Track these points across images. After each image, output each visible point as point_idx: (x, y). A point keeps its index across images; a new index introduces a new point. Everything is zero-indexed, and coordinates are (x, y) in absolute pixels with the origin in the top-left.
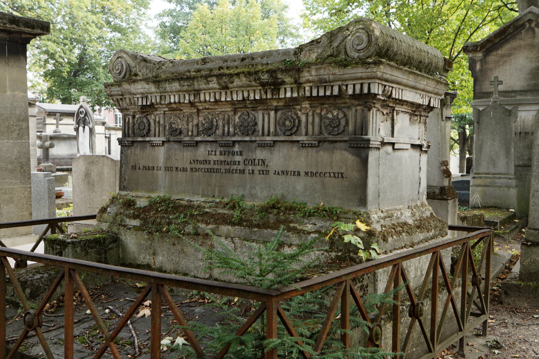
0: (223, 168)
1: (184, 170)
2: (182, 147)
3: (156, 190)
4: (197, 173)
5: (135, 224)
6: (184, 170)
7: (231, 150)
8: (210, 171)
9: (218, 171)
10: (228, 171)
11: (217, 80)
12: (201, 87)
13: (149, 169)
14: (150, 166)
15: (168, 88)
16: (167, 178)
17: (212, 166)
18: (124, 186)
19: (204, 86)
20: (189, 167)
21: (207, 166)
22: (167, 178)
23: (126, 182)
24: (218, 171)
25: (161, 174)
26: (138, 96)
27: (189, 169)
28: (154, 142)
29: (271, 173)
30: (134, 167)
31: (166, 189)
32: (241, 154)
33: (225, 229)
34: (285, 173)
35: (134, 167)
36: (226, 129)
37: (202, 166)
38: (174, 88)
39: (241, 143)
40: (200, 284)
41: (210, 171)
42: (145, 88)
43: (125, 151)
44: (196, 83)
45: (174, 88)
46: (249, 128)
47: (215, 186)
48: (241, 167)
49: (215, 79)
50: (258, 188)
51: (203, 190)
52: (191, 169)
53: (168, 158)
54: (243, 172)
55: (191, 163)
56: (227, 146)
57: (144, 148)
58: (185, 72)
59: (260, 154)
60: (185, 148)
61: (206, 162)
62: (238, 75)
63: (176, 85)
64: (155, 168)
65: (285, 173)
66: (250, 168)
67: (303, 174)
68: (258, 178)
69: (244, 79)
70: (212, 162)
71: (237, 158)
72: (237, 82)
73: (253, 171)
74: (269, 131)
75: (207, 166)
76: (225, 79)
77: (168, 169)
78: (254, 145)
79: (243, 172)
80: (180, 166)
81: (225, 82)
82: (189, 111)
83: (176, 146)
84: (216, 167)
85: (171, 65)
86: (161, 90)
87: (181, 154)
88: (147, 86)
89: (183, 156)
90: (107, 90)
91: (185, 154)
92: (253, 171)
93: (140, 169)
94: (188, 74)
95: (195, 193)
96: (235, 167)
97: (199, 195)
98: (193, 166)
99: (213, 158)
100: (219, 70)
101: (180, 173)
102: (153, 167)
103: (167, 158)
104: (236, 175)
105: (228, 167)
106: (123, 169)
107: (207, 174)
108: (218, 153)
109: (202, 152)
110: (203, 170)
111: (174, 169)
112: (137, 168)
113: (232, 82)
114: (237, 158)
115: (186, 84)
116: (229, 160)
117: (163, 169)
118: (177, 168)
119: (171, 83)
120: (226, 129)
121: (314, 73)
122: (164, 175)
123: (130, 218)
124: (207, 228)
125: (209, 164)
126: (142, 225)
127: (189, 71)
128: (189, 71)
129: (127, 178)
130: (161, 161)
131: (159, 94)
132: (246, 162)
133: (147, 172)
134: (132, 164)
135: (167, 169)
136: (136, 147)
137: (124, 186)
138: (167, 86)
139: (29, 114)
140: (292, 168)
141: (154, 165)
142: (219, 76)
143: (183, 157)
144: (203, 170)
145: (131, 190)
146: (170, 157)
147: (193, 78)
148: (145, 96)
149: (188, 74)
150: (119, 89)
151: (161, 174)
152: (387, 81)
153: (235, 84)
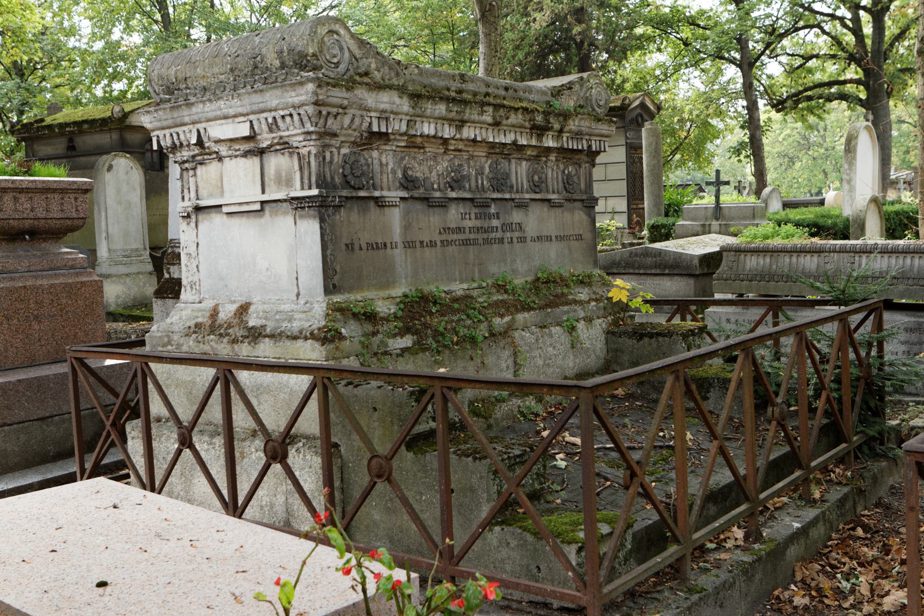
0: (481, 236)
1: (432, 244)
2: (426, 207)
3: (394, 282)
4: (450, 248)
5: (403, 345)
6: (432, 244)
7: (486, 210)
8: (466, 243)
9: (475, 242)
10: (487, 242)
11: (494, 112)
12: (472, 117)
13: (378, 248)
14: (379, 241)
15: (429, 111)
16: (409, 260)
17: (467, 236)
18: (334, 286)
19: (475, 117)
20: (438, 239)
21: (461, 237)
22: (409, 260)
23: (336, 278)
24: (475, 242)
25: (398, 254)
26: (373, 114)
27: (439, 243)
28: (387, 199)
29: (529, 239)
30: (350, 247)
31: (409, 279)
32: (498, 218)
33: (521, 317)
34: (539, 238)
35: (350, 247)
36: (480, 182)
37: (455, 237)
38: (437, 111)
39: (497, 202)
40: (602, 384)
41: (466, 243)
42: (394, 103)
43: (329, 216)
44: (468, 111)
45: (437, 111)
46: (500, 182)
47: (474, 265)
48: (499, 235)
49: (491, 109)
50: (518, 261)
51: (460, 272)
52: (442, 242)
53: (407, 227)
54: (501, 241)
55: (440, 233)
56: (480, 204)
57: (365, 211)
58: (443, 89)
59: (517, 216)
60: (431, 209)
61: (459, 230)
62: (517, 109)
63: (441, 109)
64: (389, 245)
65: (539, 238)
66: (508, 235)
67: (554, 238)
68: (517, 246)
69: (520, 116)
70: (467, 230)
71: (495, 223)
72: (514, 119)
73: (512, 238)
74: (522, 187)
75: (461, 237)
76: (502, 112)
77: (409, 245)
78: (511, 204)
79: (501, 241)
80: (426, 240)
81: (501, 116)
82: (434, 150)
83: (419, 206)
84: (472, 236)
85: (416, 71)
86: (418, 111)
87: (426, 219)
88: (397, 100)
89: (429, 221)
90: (319, 91)
91: (431, 219)
92: (512, 238)
93: (361, 249)
94: (447, 93)
95: (451, 279)
96: (493, 235)
97: (455, 281)
98: (444, 237)
99: (468, 224)
100: (485, 97)
101: (428, 252)
102: (385, 245)
103: (405, 226)
104: (495, 246)
105: (485, 236)
106: (329, 252)
107: (463, 248)
108: (473, 216)
109: (454, 214)
110: (457, 243)
111: (418, 244)
112: (356, 247)
113: (507, 118)
114: (495, 223)
115: (455, 109)
116: (486, 226)
117: (400, 245)
118: (422, 242)
119: (436, 104)
120: (480, 182)
121: (576, 123)
122: (403, 256)
123: (395, 336)
124: (499, 322)
125: (464, 232)
126: (418, 343)
127: (448, 89)
128: (448, 89)
129: (338, 269)
130: (397, 233)
131: (408, 118)
132: (504, 228)
133: (375, 253)
134: (345, 240)
135: (407, 244)
136: (351, 209)
137: (334, 286)
138: (430, 107)
139: (594, 179)
140: (545, 233)
141: (386, 240)
142: (497, 107)
143: (430, 223)
144: (457, 243)
145: (350, 290)
146: (410, 224)
147: (465, 102)
148: (384, 116)
149: (447, 93)
150: (345, 95)
151: (398, 254)
152: (602, 136)
153: (510, 121)
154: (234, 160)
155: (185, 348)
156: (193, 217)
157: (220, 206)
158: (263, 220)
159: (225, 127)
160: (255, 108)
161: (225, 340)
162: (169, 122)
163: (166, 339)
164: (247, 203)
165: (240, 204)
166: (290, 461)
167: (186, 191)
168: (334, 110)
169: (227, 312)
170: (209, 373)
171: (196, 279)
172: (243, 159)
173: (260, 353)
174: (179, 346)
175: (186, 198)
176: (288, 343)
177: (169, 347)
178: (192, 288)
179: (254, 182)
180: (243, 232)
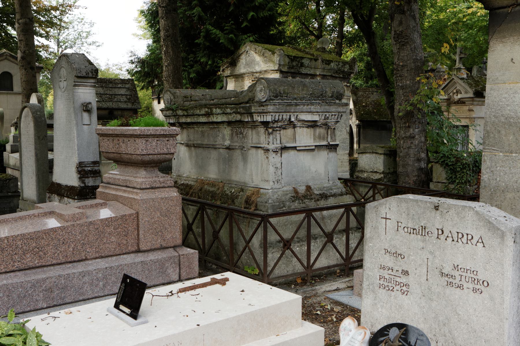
154: (302, 128)
155: (293, 207)
156: (280, 152)
157: (296, 147)
158: (314, 153)
159: (307, 116)
160: (325, 110)
161: (313, 201)
162: (283, 110)
163: (282, 205)
164: (309, 146)
165: (305, 146)
166: (334, 241)
167: (275, 140)
168: (333, 114)
169: (302, 189)
170: (342, 210)
171: (280, 178)
172: (307, 129)
173: (329, 203)
174: (289, 207)
175: (275, 143)
176: (340, 197)
177: (284, 208)
178: (278, 182)
179: (311, 138)
180: (305, 159)
